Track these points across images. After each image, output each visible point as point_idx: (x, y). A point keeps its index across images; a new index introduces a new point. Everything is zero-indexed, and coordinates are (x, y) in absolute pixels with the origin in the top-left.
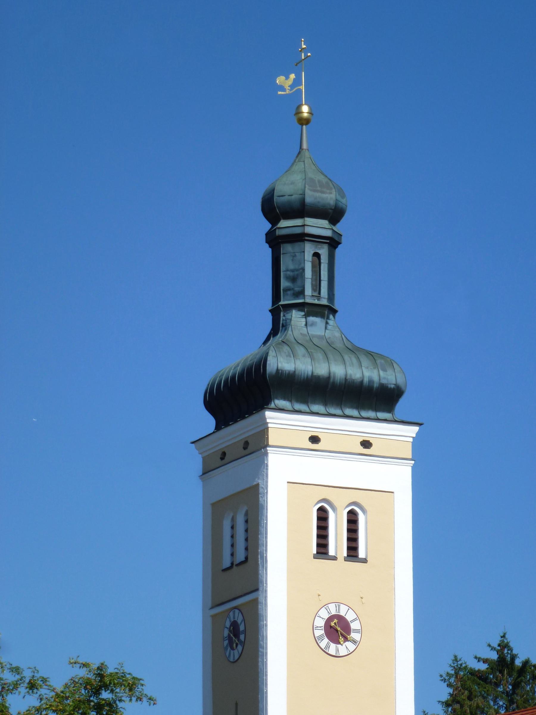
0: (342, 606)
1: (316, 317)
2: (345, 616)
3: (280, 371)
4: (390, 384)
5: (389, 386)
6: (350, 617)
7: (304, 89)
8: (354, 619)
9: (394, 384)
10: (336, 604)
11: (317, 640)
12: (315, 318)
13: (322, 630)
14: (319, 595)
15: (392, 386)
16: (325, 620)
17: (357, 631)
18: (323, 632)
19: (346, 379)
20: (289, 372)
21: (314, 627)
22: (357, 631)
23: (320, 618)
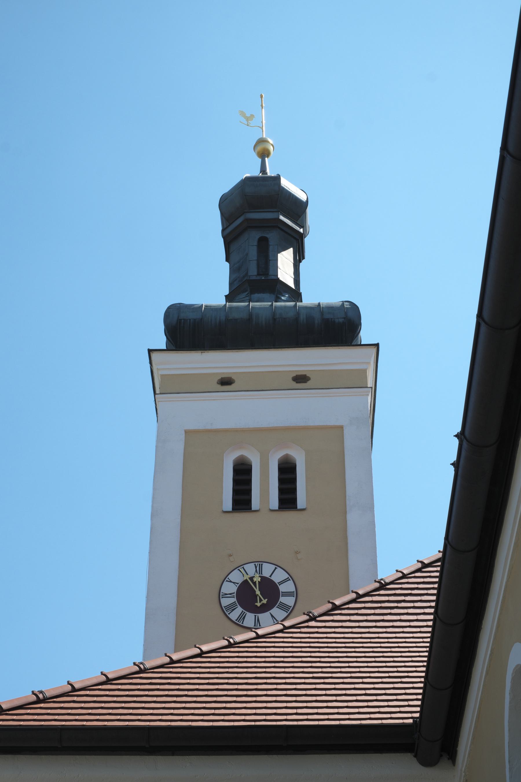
0: (245, 567)
1: (264, 293)
2: (270, 578)
3: (183, 321)
4: (338, 318)
5: (337, 321)
6: (278, 576)
7: (265, 127)
8: (284, 579)
9: (343, 318)
10: (256, 563)
11: (226, 611)
12: (262, 294)
13: (234, 597)
14: (297, 553)
15: (341, 320)
16: (238, 585)
17: (288, 594)
18: (234, 600)
19: (274, 319)
20: (195, 320)
21: (221, 594)
22: (288, 594)
23: (233, 582)
